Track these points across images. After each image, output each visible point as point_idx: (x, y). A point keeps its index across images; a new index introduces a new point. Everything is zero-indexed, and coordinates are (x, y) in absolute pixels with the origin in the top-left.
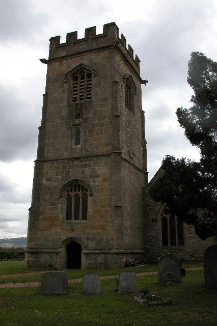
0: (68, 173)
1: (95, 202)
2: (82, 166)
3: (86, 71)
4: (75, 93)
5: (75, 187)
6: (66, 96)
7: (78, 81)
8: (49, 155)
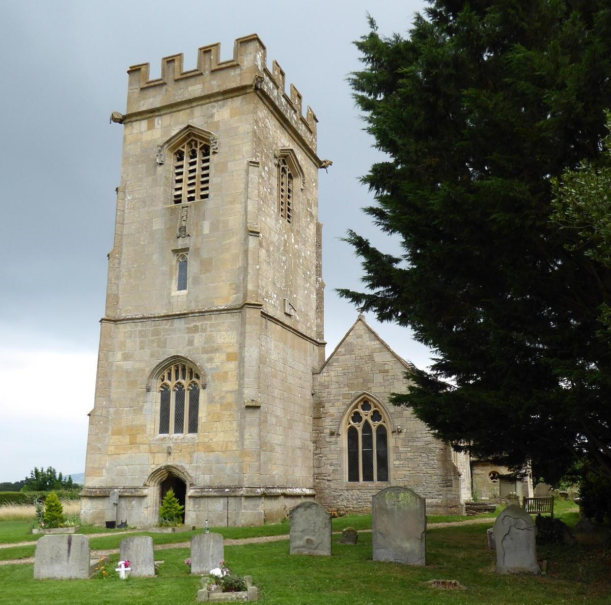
0: (163, 344)
1: (211, 401)
2: (190, 330)
3: (199, 141)
4: (178, 186)
5: (177, 372)
6: (160, 191)
7: (197, 159)
8: (107, 305)
